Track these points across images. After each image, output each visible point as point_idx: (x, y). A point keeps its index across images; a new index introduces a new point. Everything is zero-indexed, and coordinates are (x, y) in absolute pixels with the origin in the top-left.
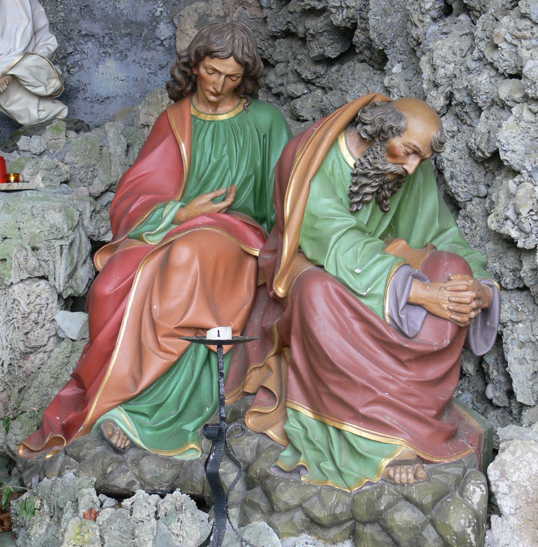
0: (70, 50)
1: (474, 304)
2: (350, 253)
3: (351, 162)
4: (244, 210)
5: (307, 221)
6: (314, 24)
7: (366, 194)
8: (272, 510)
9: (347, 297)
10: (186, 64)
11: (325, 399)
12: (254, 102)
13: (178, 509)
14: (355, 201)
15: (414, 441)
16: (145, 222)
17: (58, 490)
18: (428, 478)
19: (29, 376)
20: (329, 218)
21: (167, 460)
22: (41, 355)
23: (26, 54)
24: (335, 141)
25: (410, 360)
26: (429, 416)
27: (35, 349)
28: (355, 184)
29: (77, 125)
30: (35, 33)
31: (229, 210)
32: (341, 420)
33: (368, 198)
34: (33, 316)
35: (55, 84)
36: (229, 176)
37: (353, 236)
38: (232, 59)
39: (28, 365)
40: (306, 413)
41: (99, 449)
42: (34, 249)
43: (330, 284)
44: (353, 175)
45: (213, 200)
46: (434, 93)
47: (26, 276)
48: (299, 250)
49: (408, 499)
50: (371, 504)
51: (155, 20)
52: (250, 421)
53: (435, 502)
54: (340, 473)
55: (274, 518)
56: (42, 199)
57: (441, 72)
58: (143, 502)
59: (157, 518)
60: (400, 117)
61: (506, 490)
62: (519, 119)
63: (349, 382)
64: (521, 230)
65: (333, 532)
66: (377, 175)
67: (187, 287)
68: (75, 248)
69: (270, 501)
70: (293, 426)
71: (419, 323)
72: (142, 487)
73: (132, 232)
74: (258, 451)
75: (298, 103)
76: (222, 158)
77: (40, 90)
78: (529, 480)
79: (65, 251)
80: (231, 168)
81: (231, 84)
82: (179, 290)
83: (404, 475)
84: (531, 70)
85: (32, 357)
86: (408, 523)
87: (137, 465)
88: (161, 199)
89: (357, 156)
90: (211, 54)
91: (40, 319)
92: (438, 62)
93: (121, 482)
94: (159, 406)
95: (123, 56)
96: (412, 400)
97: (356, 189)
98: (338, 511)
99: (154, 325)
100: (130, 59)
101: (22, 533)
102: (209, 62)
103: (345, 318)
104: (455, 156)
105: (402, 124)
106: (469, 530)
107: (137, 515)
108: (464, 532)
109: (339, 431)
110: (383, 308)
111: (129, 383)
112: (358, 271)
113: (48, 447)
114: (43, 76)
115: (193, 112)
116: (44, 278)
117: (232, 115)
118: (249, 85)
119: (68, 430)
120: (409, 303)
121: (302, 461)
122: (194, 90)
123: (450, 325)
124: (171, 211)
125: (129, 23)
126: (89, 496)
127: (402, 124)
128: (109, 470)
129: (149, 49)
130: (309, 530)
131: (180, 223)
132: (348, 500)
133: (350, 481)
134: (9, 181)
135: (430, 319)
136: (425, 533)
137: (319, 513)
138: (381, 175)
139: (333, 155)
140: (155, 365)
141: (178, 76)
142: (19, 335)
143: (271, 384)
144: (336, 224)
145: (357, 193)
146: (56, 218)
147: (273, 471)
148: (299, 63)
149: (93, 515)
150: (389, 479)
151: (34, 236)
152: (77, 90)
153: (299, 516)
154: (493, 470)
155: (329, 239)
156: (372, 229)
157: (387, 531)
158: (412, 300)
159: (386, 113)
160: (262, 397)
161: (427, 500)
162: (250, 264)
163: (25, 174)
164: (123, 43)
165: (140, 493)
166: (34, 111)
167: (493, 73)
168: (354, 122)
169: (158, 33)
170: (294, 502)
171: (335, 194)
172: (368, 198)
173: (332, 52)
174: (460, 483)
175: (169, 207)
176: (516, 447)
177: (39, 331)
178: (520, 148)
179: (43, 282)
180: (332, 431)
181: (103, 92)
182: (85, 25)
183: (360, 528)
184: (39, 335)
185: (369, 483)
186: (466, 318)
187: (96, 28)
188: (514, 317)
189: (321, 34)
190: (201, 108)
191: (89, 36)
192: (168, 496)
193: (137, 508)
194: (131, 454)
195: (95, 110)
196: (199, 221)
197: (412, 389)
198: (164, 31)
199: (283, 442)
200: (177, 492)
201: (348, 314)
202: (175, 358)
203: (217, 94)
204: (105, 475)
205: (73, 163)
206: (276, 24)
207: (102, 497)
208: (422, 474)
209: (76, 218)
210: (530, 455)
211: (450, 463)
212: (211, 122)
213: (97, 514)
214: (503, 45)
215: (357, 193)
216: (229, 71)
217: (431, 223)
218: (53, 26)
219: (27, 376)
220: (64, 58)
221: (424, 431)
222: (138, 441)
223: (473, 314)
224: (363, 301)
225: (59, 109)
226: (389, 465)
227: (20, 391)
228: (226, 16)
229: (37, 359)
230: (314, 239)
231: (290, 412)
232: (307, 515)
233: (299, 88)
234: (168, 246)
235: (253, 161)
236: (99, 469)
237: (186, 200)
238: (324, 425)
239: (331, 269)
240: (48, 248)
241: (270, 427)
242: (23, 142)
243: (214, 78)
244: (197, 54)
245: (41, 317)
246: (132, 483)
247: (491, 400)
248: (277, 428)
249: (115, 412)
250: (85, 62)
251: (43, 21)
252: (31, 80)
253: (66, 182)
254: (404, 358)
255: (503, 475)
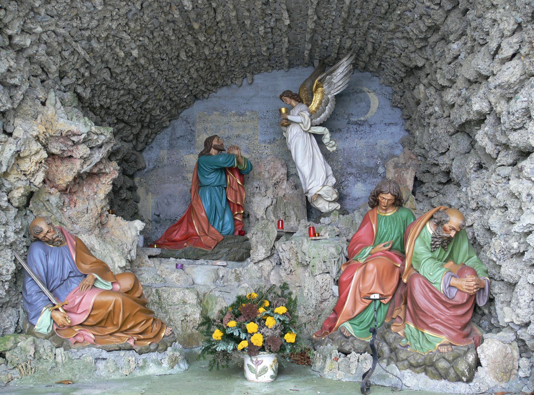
0: (343, 180)
1: (475, 287)
2: (429, 267)
3: (431, 232)
4: (397, 249)
5: (414, 255)
6: (434, 170)
7: (437, 245)
8: (397, 361)
9: (427, 283)
10: (374, 196)
11: (418, 321)
12: (401, 208)
13: (366, 359)
14: (433, 247)
15: (450, 337)
16: (359, 255)
17: (325, 350)
18: (452, 351)
19: (323, 310)
20: (422, 254)
21: (363, 341)
22: (327, 302)
23: (323, 186)
24: (425, 225)
25: (450, 307)
26: (457, 329)
27: (325, 300)
28: (433, 241)
29: (343, 212)
30: (327, 177)
31: (390, 250)
32: (423, 329)
33: (438, 246)
34: (324, 287)
35: (335, 196)
36: (391, 236)
37: (430, 261)
38: (389, 194)
39: (322, 306)
40: (412, 326)
41: (340, 336)
42: (324, 262)
43: (420, 279)
44: (432, 237)
45: (384, 246)
46: (472, 202)
47: (322, 272)
48: (411, 266)
49: (444, 358)
50: (431, 359)
51: (377, 166)
52: (393, 328)
53: (454, 360)
54: (422, 348)
55: (398, 364)
56: (327, 243)
57: (474, 194)
58: (353, 356)
59: (358, 362)
60: (447, 216)
61: (484, 357)
62: (497, 215)
63: (426, 315)
64: (497, 258)
65: (418, 369)
66: (440, 238)
67: (372, 279)
68: (340, 261)
69: (397, 357)
70: (407, 330)
71: (455, 294)
72: (354, 351)
73: (354, 258)
74: (395, 338)
75: (432, 200)
76: (388, 230)
77: (329, 199)
78: (493, 354)
79: (336, 263)
80: (391, 233)
81: (390, 202)
82: (369, 281)
83: (443, 349)
84: (499, 196)
85: (324, 303)
86: (443, 367)
87: (353, 343)
88: (366, 246)
89: (433, 230)
90: (382, 192)
91: (327, 289)
92: (473, 190)
93: (347, 348)
94: (362, 322)
95: (364, 181)
96: (451, 322)
97: (433, 243)
98: (419, 361)
99: (360, 292)
100: (367, 182)
101: (313, 365)
102: (381, 195)
103: (426, 291)
104: (479, 227)
105: (448, 219)
106: (466, 370)
107: (351, 360)
108: (464, 371)
109: (423, 333)
110: (441, 287)
111: (351, 313)
112: (431, 274)
113: (323, 335)
114: (330, 194)
115: (378, 213)
116: (328, 273)
117: (392, 213)
118: (398, 203)
119: (330, 329)
120: (450, 286)
121: (408, 343)
122: (378, 204)
123: (466, 294)
124: (368, 250)
125: (367, 168)
126: (335, 353)
127: (448, 219)
128: (343, 344)
129: (375, 178)
130: (410, 368)
131: (372, 254)
132: (423, 357)
133: (425, 351)
134: (315, 236)
135: (459, 292)
136: (450, 371)
137: (413, 362)
138: (442, 237)
139: (424, 230)
140: (360, 307)
141: (371, 200)
142: (319, 295)
143: (401, 315)
144: (424, 256)
145: (433, 244)
146: (333, 250)
147: (398, 346)
148: (433, 184)
149: (336, 359)
150: (438, 351)
151: (324, 257)
152: (346, 196)
153: (406, 363)
154: (479, 350)
155: (421, 262)
156: (441, 257)
157: (436, 369)
158: (451, 285)
159: (443, 215)
160: (398, 320)
161: (451, 359)
162: (397, 270)
163: (322, 233)
164: (364, 176)
165: (353, 353)
166: (327, 207)
167: (490, 196)
168: (432, 217)
169: (378, 171)
170: (404, 358)
171: (425, 244)
172: (438, 246)
173: (444, 180)
174: (465, 353)
175: (368, 248)
176: (488, 341)
177: (326, 293)
178: (498, 226)
179: (328, 275)
180: (420, 332)
181: (357, 197)
182: (349, 170)
183: (427, 368)
184: (327, 295)
185: (431, 352)
186: (472, 292)
187: (354, 171)
188: (500, 292)
189: (439, 173)
190: (381, 211)
191: (351, 174)
192: (363, 354)
193: (351, 358)
194: (351, 338)
195: (353, 203)
196: (378, 254)
197: (450, 318)
198: (381, 170)
199: (404, 336)
200: (366, 353)
201: (427, 290)
202: (367, 305)
203: (385, 207)
204: (341, 346)
205: (341, 227)
206: (423, 168)
207: (340, 353)
208: (450, 349)
209: (340, 250)
210: (494, 344)
211: (462, 346)
212: (384, 216)
213: (338, 359)
214: (492, 185)
215: (433, 244)
216: (389, 198)
217: (465, 255)
218: (334, 175)
219: (322, 310)
220: (341, 183)
221: (454, 334)
222: (353, 334)
223: (475, 290)
224: (433, 285)
225: (337, 206)
226: (439, 346)
227: (319, 316)
228: (405, 164)
229: (325, 304)
230: (416, 262)
231: (406, 325)
232: (409, 362)
233: (433, 194)
234: (366, 263)
235: (400, 231)
236: (339, 343)
237: (375, 246)
238: (418, 330)
239: (421, 273)
240: (330, 262)
241: (399, 331)
242: (322, 220)
243: (384, 200)
244: (377, 192)
245: (327, 288)
246: (351, 349)
247: (493, 324)
248: (402, 331)
249: (346, 323)
250: (349, 185)
251: (330, 172)
252: (326, 196)
253: (338, 235)
254: (448, 306)
255: (483, 351)
